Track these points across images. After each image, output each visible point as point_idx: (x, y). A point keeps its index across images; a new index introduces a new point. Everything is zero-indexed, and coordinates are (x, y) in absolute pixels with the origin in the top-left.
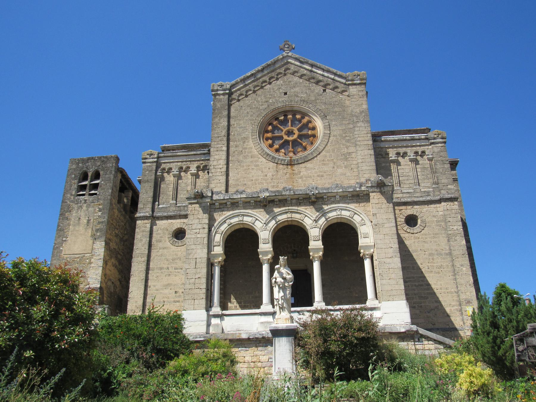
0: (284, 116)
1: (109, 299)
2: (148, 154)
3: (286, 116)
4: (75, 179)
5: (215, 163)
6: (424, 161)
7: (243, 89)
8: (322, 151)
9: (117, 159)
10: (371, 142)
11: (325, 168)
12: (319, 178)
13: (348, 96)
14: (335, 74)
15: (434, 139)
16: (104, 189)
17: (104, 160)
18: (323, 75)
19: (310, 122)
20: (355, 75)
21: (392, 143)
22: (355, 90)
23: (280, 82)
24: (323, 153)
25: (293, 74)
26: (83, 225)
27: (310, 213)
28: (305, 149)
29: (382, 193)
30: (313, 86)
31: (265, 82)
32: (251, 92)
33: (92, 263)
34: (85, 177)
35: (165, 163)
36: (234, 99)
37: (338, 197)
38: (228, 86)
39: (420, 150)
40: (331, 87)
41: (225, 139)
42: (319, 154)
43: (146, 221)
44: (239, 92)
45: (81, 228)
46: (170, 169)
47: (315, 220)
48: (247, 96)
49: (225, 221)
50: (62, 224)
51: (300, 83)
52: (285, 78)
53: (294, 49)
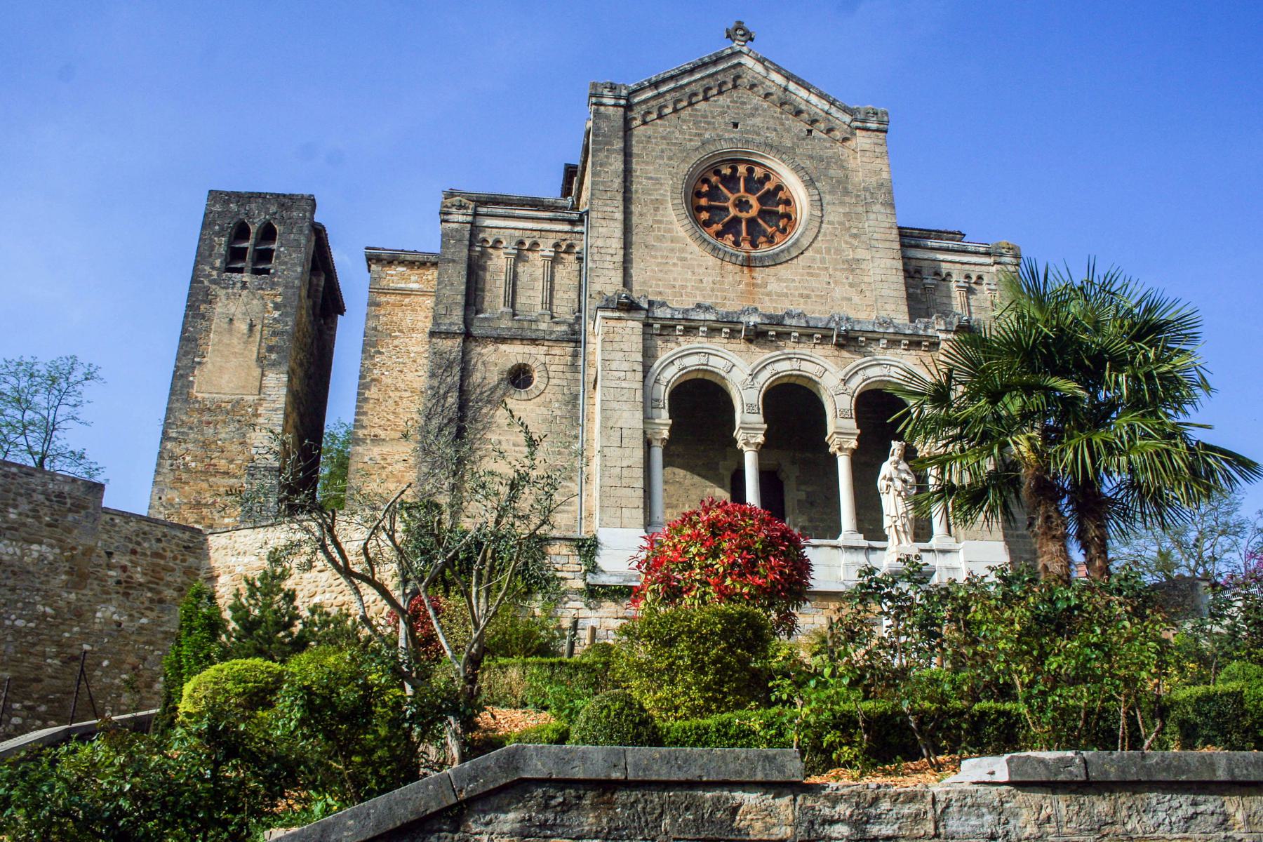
0: (730, 168)
5: (600, 243)
8: (807, 249)
9: (312, 202)
10: (897, 246)
11: (814, 283)
17: (286, 201)
22: (868, 141)
23: (723, 100)
28: (771, 241)
30: (788, 120)
33: (260, 415)
41: (620, 197)
42: (802, 253)
44: (644, 107)
45: (235, 341)
49: (672, 362)
51: (764, 110)
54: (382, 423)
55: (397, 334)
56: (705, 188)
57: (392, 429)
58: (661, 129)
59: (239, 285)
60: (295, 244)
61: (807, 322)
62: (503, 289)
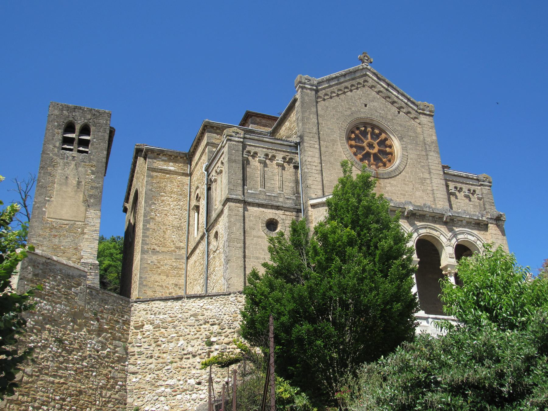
2: (234, 132)
3: (366, 128)
4: (59, 127)
5: (309, 159)
6: (474, 198)
7: (328, 90)
8: (402, 171)
12: (402, 197)
13: (419, 123)
14: (409, 100)
15: (483, 181)
16: (97, 148)
18: (397, 97)
19: (386, 139)
20: (425, 106)
21: (452, 176)
22: (425, 120)
23: (359, 92)
24: (403, 173)
25: (371, 88)
26: (72, 187)
27: (445, 232)
28: (385, 165)
29: (498, 226)
31: (346, 88)
32: (335, 95)
33: (85, 233)
34: (70, 128)
35: (250, 145)
36: (320, 97)
37: (464, 222)
38: (315, 83)
39: (472, 188)
40: (404, 110)
42: (400, 173)
43: (238, 205)
45: (69, 190)
46: (256, 153)
47: (449, 239)
48: (331, 98)
50: (44, 180)
51: (378, 99)
52: (364, 89)
53: (371, 62)
54: (157, 243)
55: (163, 194)
56: (353, 136)
57: (162, 246)
58: (332, 104)
59: (71, 158)
60: (102, 138)
61: (433, 210)
62: (259, 178)
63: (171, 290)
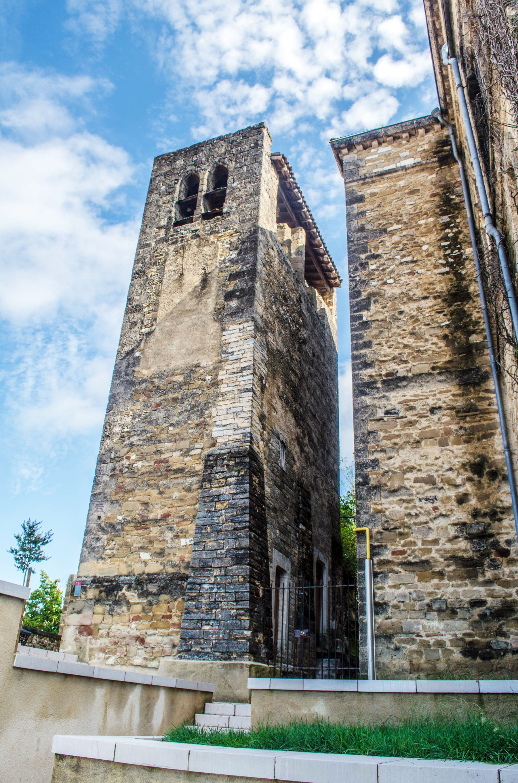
1: (277, 491)
63: (462, 490)
